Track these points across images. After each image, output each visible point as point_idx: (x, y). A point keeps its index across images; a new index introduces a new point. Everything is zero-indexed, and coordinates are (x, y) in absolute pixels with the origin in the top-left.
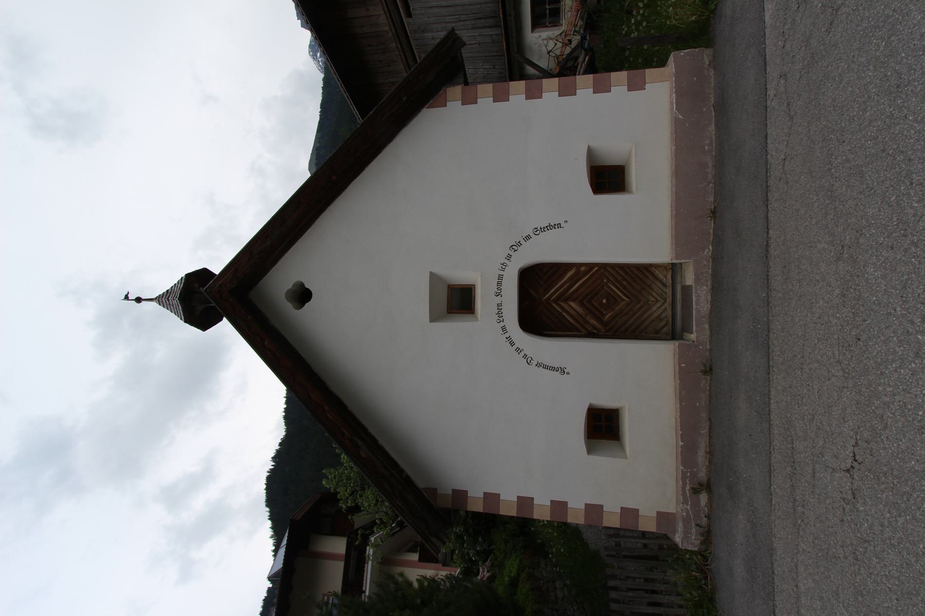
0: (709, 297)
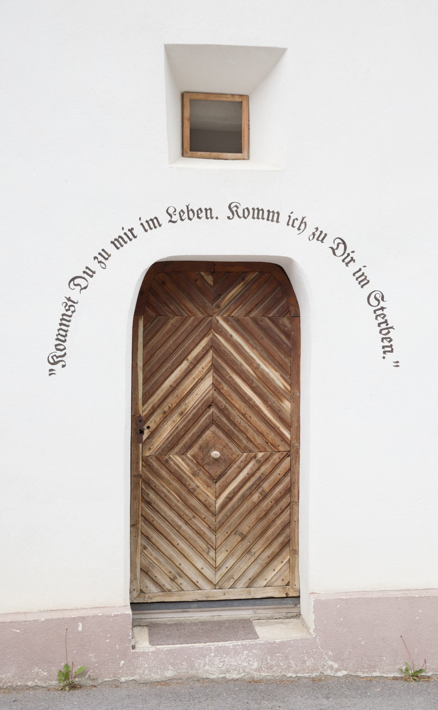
0: (235, 676)
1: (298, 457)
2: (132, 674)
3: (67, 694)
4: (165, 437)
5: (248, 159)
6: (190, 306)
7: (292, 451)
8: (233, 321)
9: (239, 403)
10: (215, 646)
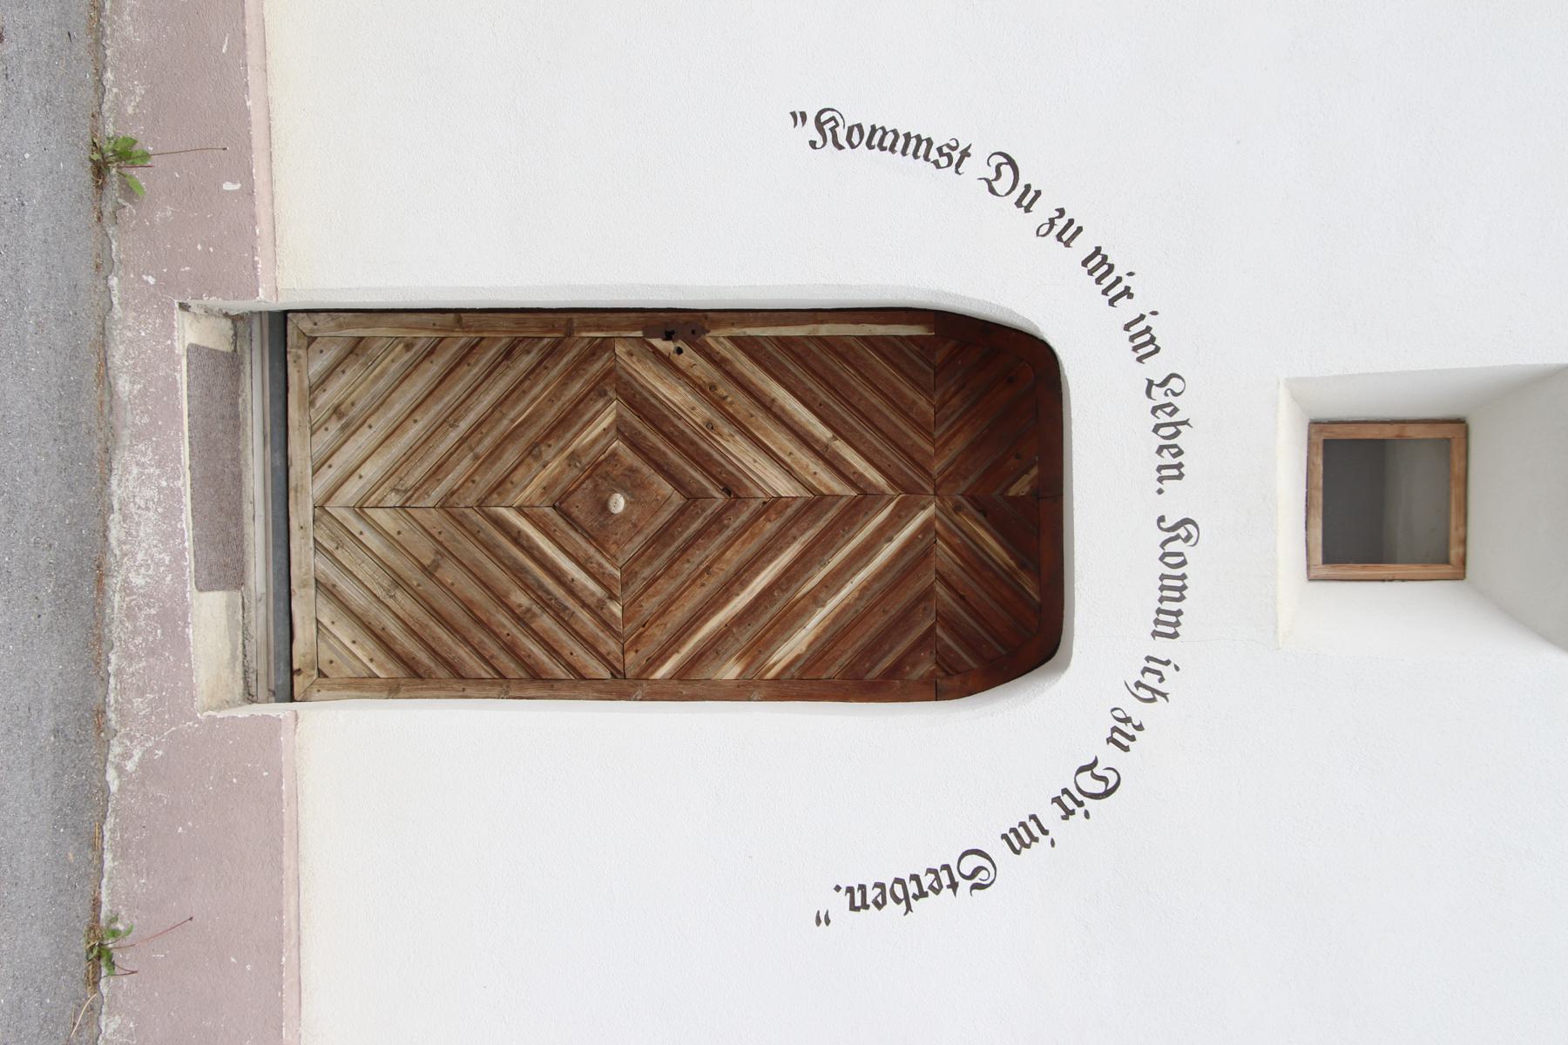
0: (114, 534)
1: (611, 697)
2: (125, 302)
3: (85, 153)
4: (656, 388)
5: (1311, 580)
6: (959, 444)
7: (625, 682)
8: (924, 543)
9: (734, 557)
10: (183, 488)
